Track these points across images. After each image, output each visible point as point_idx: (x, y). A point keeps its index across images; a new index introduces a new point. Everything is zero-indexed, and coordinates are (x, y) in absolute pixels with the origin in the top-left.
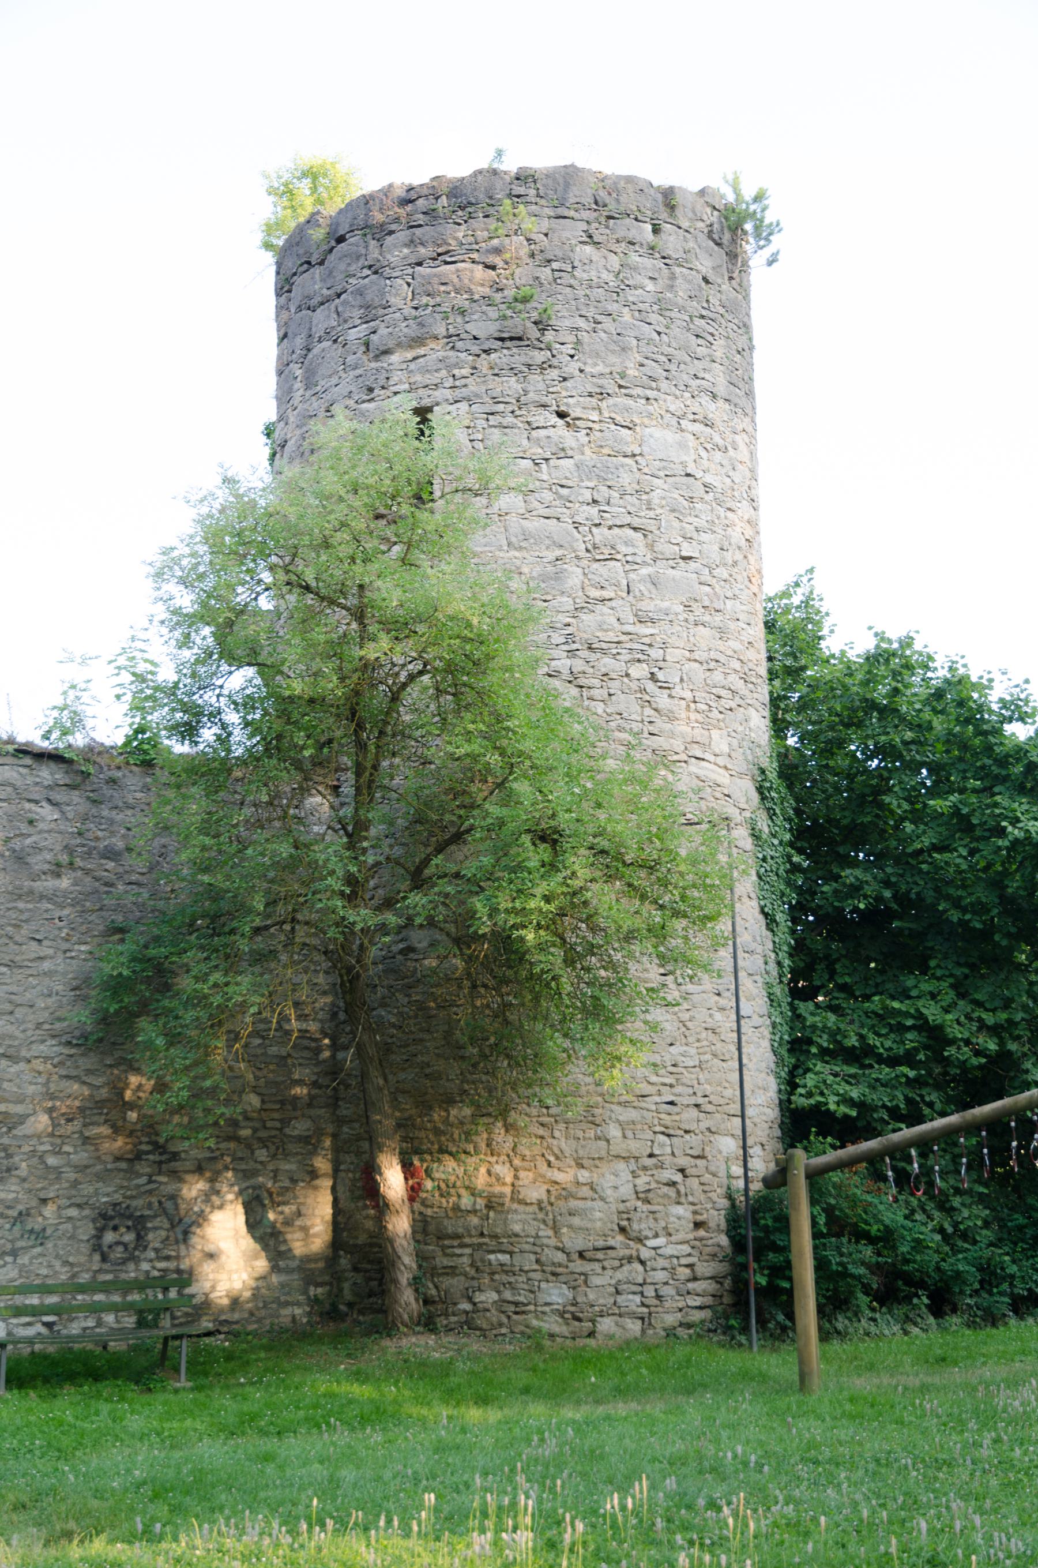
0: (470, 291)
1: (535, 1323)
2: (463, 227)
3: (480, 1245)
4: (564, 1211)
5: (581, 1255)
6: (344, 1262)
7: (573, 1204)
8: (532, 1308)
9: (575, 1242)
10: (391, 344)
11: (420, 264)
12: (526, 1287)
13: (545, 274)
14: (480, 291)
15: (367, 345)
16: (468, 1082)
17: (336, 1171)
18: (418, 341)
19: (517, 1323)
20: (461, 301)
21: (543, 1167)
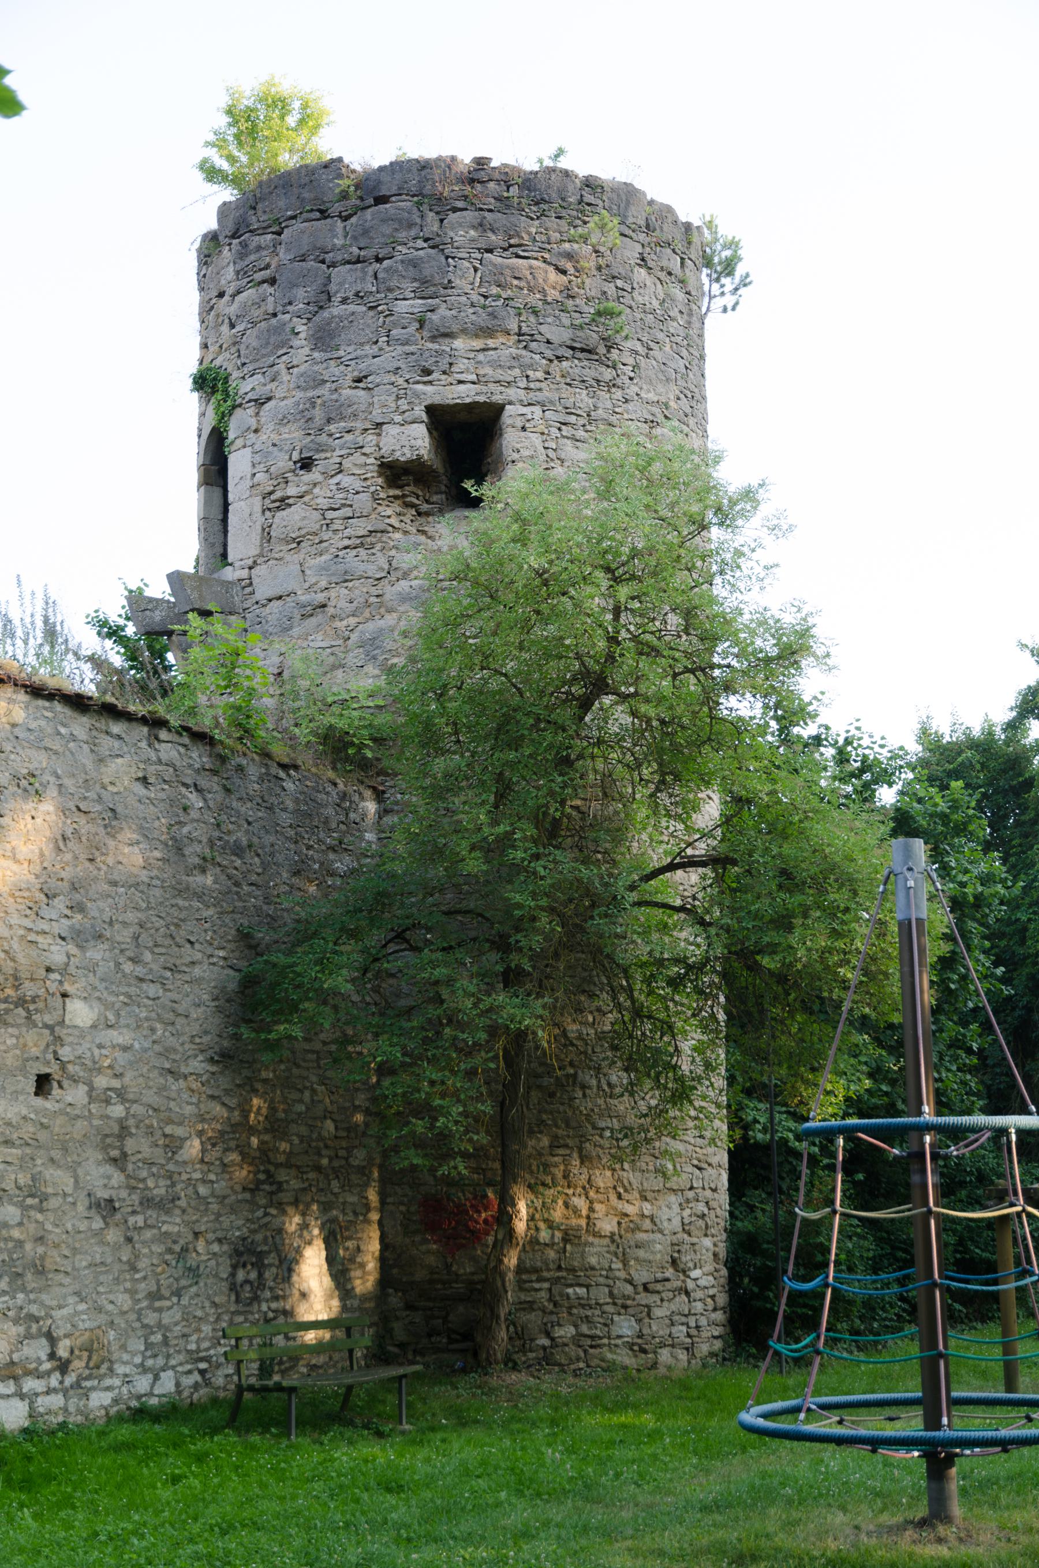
0: (543, 292)
1: (609, 1356)
2: (537, 223)
3: (559, 1278)
4: (632, 1243)
5: (646, 1289)
6: (395, 1300)
7: (641, 1236)
8: (605, 1341)
9: (642, 1276)
10: (455, 328)
11: (490, 251)
12: (601, 1320)
13: (610, 289)
14: (553, 294)
15: (422, 323)
16: (546, 1112)
17: (383, 1202)
18: (487, 332)
19: (594, 1356)
20: (535, 299)
21: (613, 1197)
